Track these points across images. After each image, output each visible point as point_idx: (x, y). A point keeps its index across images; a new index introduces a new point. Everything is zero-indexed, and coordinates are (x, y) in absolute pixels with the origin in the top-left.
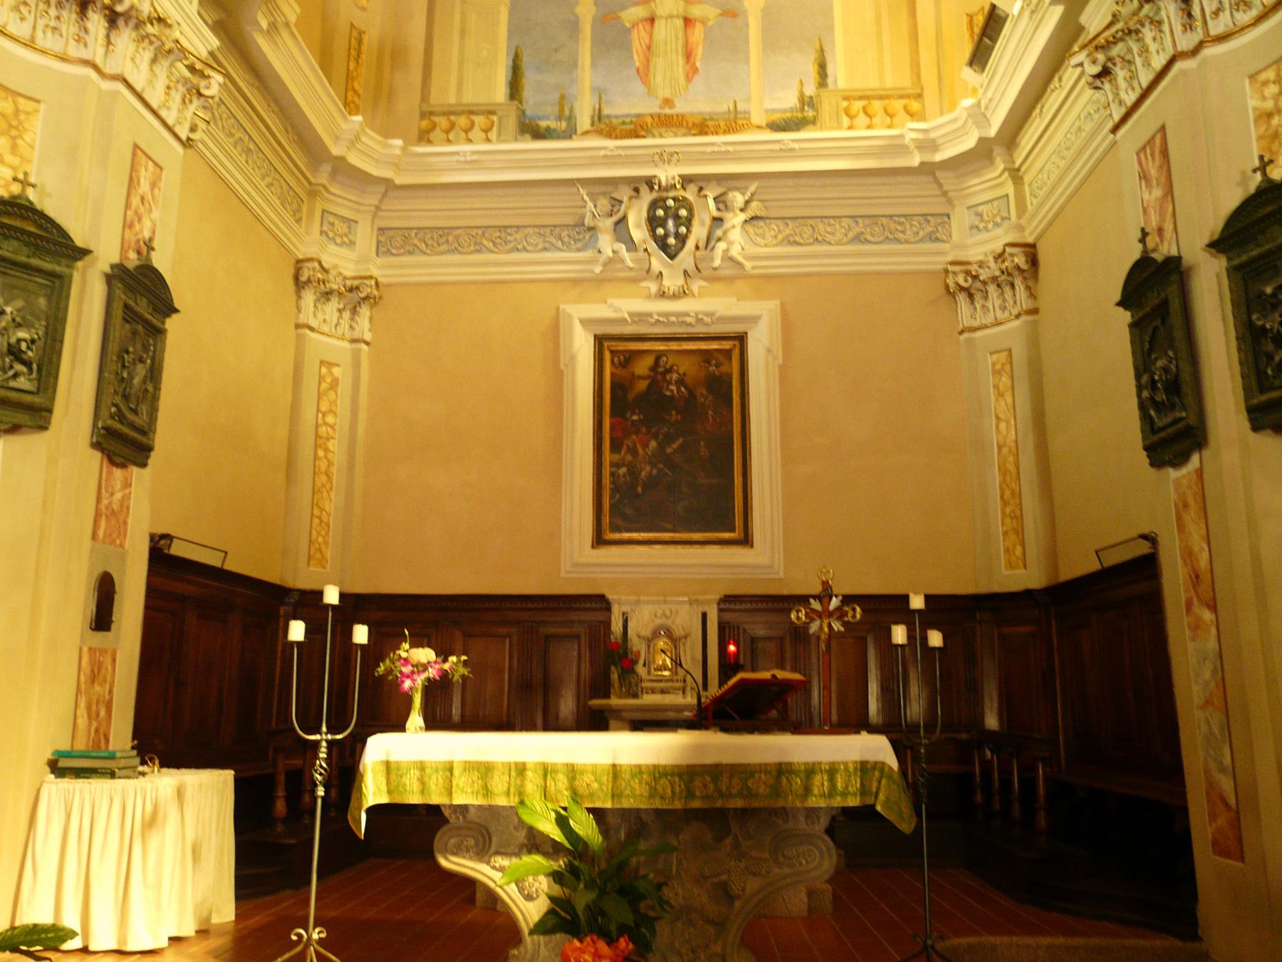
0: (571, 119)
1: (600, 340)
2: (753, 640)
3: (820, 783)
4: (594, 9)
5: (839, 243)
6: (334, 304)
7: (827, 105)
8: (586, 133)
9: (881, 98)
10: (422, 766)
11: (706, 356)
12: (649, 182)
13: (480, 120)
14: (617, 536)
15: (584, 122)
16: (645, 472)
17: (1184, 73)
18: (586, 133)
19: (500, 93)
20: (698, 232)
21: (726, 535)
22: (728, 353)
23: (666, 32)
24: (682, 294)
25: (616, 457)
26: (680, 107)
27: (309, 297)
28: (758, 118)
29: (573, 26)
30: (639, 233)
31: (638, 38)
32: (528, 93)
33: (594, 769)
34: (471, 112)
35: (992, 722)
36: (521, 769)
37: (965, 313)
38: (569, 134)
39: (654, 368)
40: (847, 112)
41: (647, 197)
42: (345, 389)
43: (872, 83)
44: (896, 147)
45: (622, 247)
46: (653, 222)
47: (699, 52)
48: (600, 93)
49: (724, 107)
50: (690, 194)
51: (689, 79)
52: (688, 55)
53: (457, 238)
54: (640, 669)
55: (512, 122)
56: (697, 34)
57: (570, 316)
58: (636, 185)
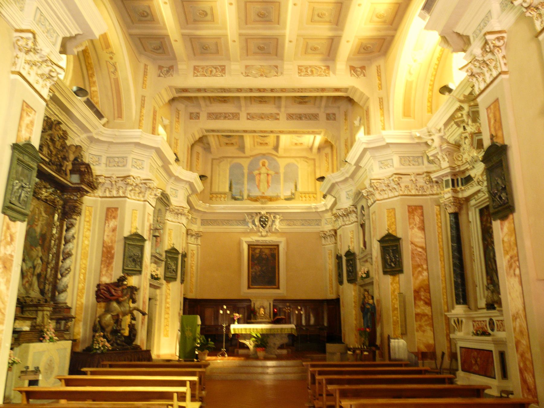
0: (242, 196)
1: (249, 246)
2: (280, 308)
3: (286, 330)
4: (247, 171)
5: (299, 225)
6: (194, 237)
7: (297, 195)
8: (246, 199)
9: (308, 194)
10: (238, 329)
11: (271, 249)
12: (260, 213)
13: (223, 196)
14: (252, 287)
15: (245, 197)
16: (258, 273)
17: (343, 229)
18: (246, 199)
19: (227, 190)
20: (270, 223)
21: (274, 287)
22: (275, 249)
23: (263, 177)
24: (266, 236)
25: (252, 271)
26: (266, 194)
27: (189, 236)
28: (282, 197)
29: (243, 174)
30: (257, 223)
31: (257, 178)
32: (233, 190)
33: (259, 329)
34: (221, 194)
35: (326, 324)
36: (250, 329)
37: (323, 241)
38: (242, 199)
39: (260, 252)
40: (301, 197)
41: (259, 216)
42: (196, 255)
43: (306, 190)
44: (310, 208)
45: (254, 226)
46: (260, 221)
47: (270, 182)
48: (249, 190)
49: (275, 195)
50: (268, 216)
51: (268, 188)
52: (268, 182)
53: (219, 223)
54: (258, 314)
55: (230, 197)
56: (270, 177)
57: (242, 241)
58: (257, 214)
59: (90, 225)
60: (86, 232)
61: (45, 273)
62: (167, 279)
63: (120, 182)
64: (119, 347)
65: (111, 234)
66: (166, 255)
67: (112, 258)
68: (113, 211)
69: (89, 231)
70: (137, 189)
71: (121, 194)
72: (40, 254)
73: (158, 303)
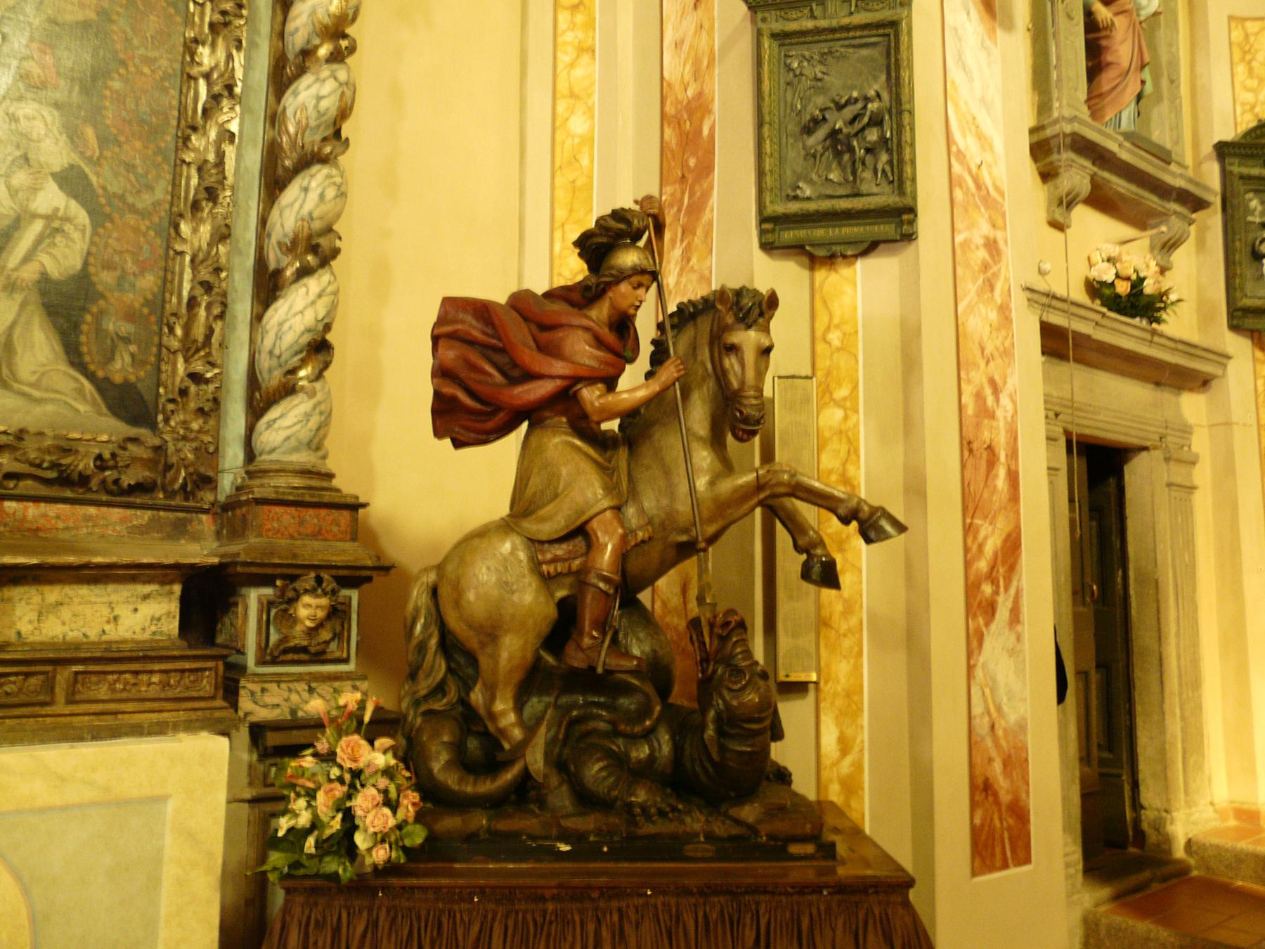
59: (590, 25)
60: (572, 65)
62: (1250, 322)
64: (587, 823)
66: (1225, 174)
67: (706, 169)
69: (586, 58)
73: (1202, 475)
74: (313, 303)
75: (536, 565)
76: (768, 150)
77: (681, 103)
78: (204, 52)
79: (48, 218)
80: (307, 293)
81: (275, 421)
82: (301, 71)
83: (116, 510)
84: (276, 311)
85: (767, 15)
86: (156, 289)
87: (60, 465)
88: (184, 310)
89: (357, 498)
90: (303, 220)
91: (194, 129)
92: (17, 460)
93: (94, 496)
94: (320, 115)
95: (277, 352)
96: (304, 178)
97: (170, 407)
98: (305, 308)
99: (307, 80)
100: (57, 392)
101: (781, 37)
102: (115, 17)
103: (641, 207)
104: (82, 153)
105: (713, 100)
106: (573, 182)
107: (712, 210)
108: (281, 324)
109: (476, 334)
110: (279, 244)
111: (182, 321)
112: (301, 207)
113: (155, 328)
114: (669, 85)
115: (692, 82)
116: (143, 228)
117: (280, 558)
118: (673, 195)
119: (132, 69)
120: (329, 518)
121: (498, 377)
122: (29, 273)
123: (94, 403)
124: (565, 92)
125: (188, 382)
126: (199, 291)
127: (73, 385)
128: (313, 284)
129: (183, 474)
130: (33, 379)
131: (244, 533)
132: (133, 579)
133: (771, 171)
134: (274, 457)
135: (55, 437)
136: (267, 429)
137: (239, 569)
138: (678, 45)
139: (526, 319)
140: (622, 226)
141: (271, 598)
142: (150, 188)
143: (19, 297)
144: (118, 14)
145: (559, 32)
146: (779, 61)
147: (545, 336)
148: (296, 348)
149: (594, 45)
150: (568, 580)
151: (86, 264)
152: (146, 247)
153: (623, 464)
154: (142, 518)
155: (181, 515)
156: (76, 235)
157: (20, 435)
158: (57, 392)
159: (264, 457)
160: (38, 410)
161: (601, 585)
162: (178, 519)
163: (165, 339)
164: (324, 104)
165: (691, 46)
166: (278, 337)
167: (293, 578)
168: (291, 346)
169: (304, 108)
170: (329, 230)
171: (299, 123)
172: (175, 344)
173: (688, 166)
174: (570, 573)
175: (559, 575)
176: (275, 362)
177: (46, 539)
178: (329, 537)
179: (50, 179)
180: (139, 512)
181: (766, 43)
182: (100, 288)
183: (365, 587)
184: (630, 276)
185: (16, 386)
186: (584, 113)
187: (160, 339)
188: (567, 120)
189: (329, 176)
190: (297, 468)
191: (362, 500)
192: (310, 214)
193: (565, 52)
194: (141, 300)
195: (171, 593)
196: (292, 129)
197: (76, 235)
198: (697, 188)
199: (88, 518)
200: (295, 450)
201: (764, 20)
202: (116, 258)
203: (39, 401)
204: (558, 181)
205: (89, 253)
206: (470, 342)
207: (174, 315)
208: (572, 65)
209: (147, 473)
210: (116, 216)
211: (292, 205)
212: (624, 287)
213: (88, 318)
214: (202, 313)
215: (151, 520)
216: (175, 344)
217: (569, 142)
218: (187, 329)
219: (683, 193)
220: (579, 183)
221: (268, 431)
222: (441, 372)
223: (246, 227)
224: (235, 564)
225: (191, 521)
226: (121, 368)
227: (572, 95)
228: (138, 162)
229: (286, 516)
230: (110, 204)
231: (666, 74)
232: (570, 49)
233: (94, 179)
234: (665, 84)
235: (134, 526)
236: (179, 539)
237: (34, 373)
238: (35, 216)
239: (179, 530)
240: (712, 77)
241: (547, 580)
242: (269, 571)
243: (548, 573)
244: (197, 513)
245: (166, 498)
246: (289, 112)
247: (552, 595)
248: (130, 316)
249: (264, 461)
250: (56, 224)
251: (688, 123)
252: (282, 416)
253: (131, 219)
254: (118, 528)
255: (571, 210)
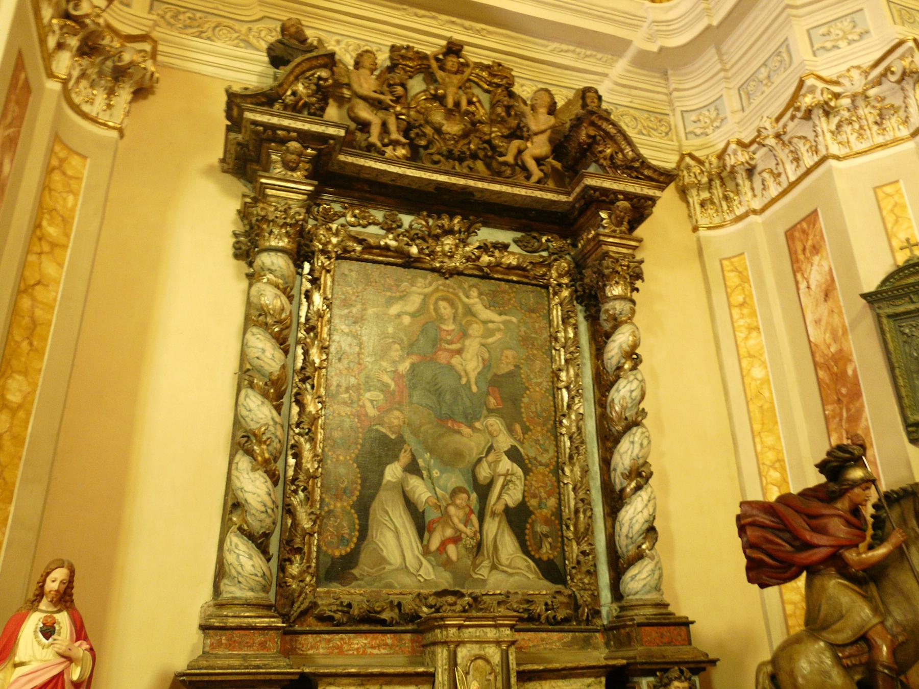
59: (753, 314)
60: (746, 338)
61: (552, 502)
63: (791, 125)
65: (824, 309)
67: (856, 394)
68: (804, 232)
69: (754, 334)
70: (864, 111)
71: (808, 160)
72: (504, 441)
74: (647, 505)
75: (838, 660)
76: (902, 384)
77: (827, 356)
78: (563, 375)
79: (506, 475)
80: (642, 500)
81: (635, 576)
82: (618, 377)
83: (555, 633)
84: (627, 512)
85: (881, 305)
86: (556, 505)
87: (529, 610)
88: (573, 516)
89: (687, 618)
90: (634, 459)
91: (564, 415)
92: (508, 609)
93: (543, 627)
94: (633, 400)
95: (630, 535)
96: (630, 436)
97: (574, 571)
98: (643, 509)
99: (622, 383)
100: (519, 569)
101: (893, 317)
102: (521, 366)
103: (852, 440)
104: (515, 438)
105: (851, 354)
106: (761, 407)
107: (867, 420)
108: (631, 519)
109: (768, 522)
110: (622, 474)
111: (573, 522)
112: (632, 453)
113: (559, 527)
114: (816, 345)
115: (832, 343)
116: (547, 473)
117: (657, 658)
118: (833, 411)
119: (532, 390)
120: (675, 632)
121: (788, 547)
122: (500, 507)
123: (536, 573)
124: (746, 354)
125: (581, 558)
126: (580, 505)
127: (526, 564)
128: (644, 494)
129: (586, 610)
130: (507, 563)
131: (630, 643)
132: (583, 676)
133: (907, 396)
134: (637, 597)
135: (523, 594)
136: (631, 580)
137: (639, 667)
138: (817, 322)
139: (797, 512)
140: (847, 455)
141: (655, 683)
142: (547, 451)
143: (497, 519)
144: (522, 364)
145: (734, 320)
146: (896, 331)
147: (814, 522)
148: (641, 532)
149: (758, 325)
150: (861, 669)
151: (524, 497)
152: (549, 482)
153: (876, 594)
154: (568, 637)
155: (586, 634)
156: (518, 482)
157: (508, 595)
158: (519, 569)
159: (631, 597)
160: (511, 579)
161: (886, 671)
162: (585, 637)
163: (564, 532)
164: (634, 394)
165: (827, 323)
166: (631, 527)
167: (665, 671)
168: (638, 532)
169: (624, 398)
170: (646, 463)
171: (622, 406)
172: (571, 535)
173: (841, 394)
174: (861, 664)
175: (854, 665)
176: (629, 541)
177: (525, 653)
178: (677, 643)
179: (504, 454)
180: (566, 634)
181: (885, 321)
182: (531, 508)
183: (702, 674)
184: (860, 484)
185: (501, 567)
186: (760, 366)
187: (562, 533)
188: (749, 370)
189: (643, 433)
190: (654, 603)
191: (691, 619)
192: (637, 455)
193: (741, 332)
194: (550, 512)
195: (601, 682)
196: (617, 408)
197: (518, 482)
198: (851, 406)
199: (542, 640)
200: (649, 592)
201: (879, 308)
202: (537, 491)
203: (511, 575)
204: (752, 407)
205: (524, 491)
206: (763, 526)
207: (569, 519)
208: (746, 338)
209: (568, 611)
210: (534, 468)
211: (626, 452)
212: (857, 490)
213: (528, 526)
214: (582, 516)
215: (572, 638)
216: (571, 535)
217: (753, 383)
218: (576, 526)
219: (841, 409)
220: (766, 407)
221: (633, 582)
222: (748, 546)
223: (593, 464)
224: (636, 663)
225: (591, 637)
226: (546, 551)
227: (750, 356)
228: (540, 438)
229: (652, 632)
230: (530, 463)
231: (812, 339)
232: (743, 329)
233: (521, 450)
234: (812, 345)
235: (565, 642)
236: (587, 649)
237: (508, 559)
238: (500, 475)
239: (586, 643)
240: (847, 340)
241: (847, 669)
242: (654, 667)
243: (848, 665)
244: (594, 632)
245: (577, 624)
246: (616, 401)
247: (853, 679)
248: (547, 522)
249: (632, 600)
250: (509, 478)
251: (835, 368)
252: (639, 572)
253: (541, 468)
254: (557, 644)
255: (763, 424)
